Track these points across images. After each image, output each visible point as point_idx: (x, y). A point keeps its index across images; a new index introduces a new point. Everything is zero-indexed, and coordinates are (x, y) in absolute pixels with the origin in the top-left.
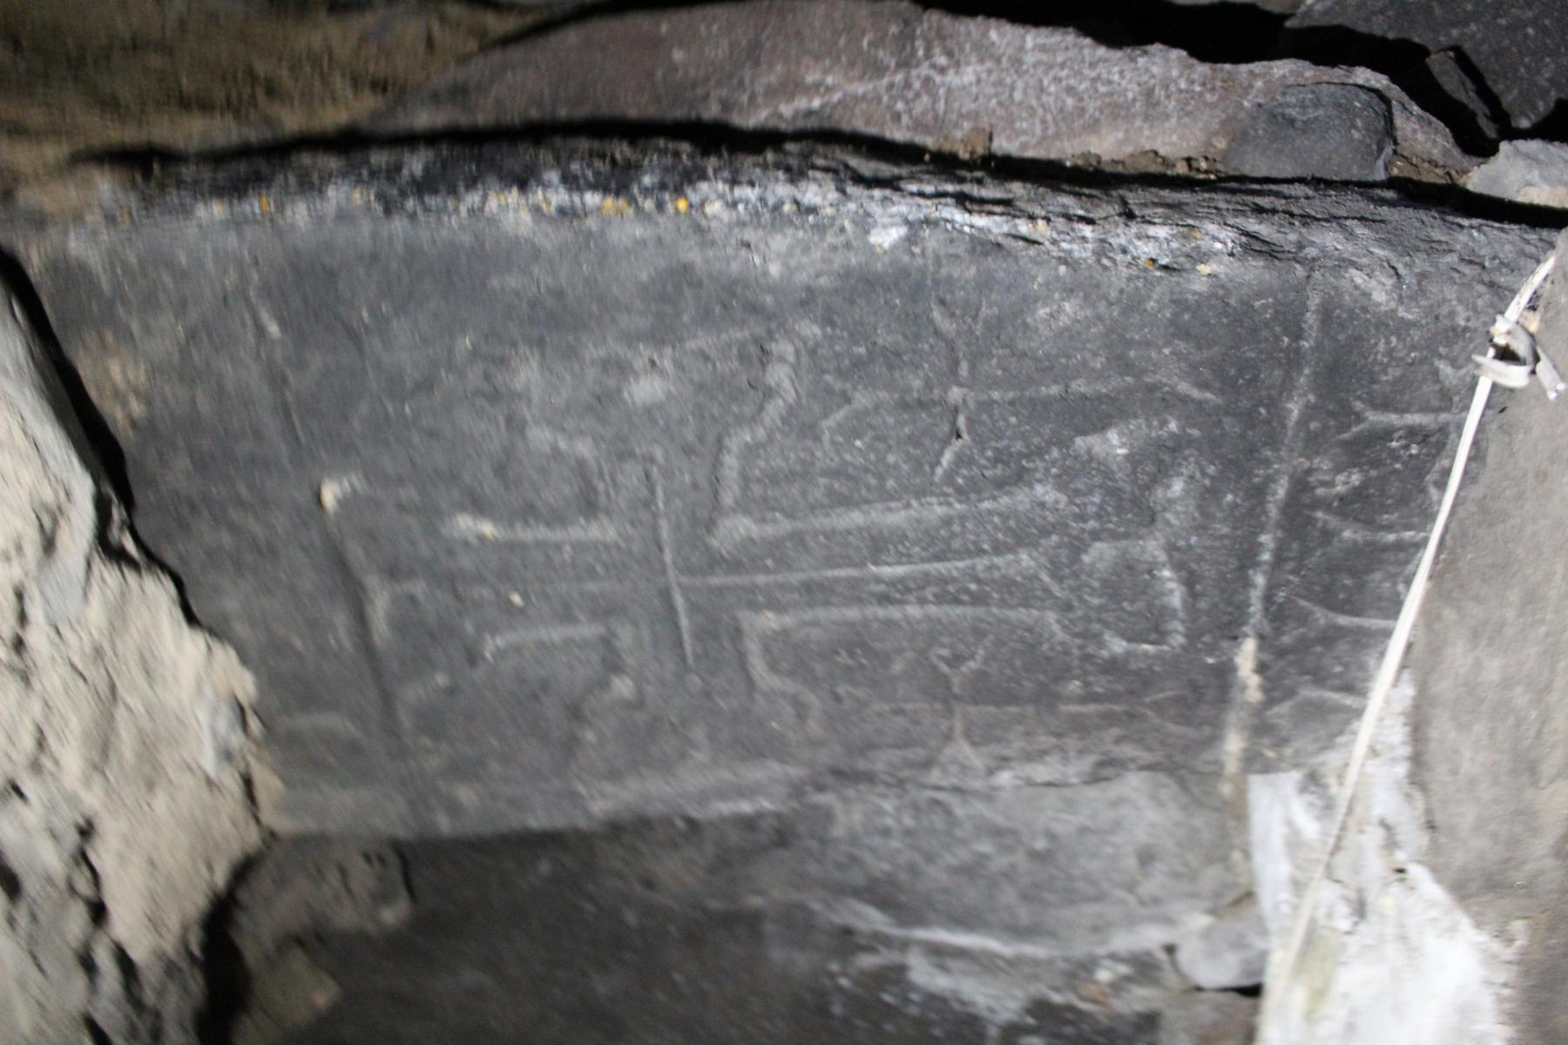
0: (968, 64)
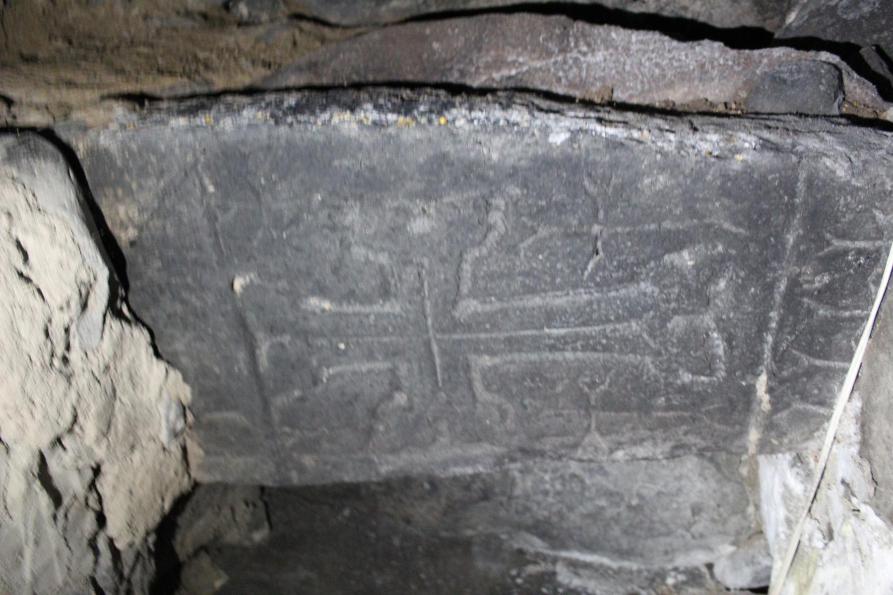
0: (599, 50)
